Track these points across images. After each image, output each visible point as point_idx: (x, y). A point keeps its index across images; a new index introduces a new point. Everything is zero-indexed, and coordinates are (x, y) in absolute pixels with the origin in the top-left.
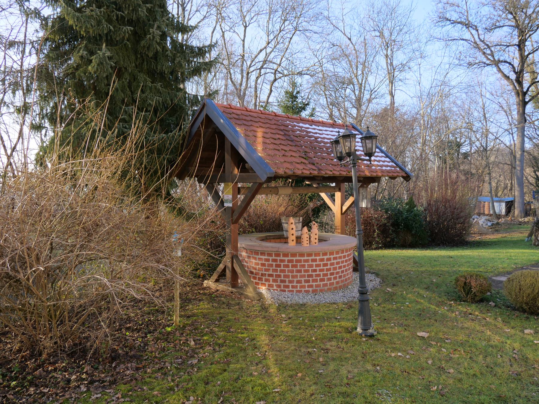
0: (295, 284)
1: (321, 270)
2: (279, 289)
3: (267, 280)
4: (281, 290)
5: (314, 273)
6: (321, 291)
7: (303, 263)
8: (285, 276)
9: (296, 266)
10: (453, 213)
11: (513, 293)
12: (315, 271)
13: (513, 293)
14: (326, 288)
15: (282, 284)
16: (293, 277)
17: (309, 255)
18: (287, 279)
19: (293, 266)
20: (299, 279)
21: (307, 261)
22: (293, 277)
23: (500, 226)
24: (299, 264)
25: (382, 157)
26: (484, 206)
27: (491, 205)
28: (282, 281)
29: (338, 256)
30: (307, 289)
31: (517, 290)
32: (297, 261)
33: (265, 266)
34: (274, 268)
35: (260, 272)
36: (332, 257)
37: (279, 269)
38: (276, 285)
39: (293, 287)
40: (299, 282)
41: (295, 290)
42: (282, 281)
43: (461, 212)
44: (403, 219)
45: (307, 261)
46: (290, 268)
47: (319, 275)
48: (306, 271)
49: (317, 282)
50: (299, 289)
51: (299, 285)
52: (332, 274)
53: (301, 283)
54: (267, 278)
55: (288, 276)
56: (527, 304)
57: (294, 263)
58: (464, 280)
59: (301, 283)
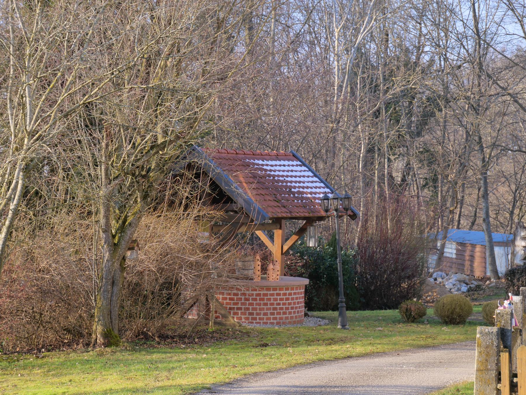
0: (262, 316)
1: (284, 304)
2: (247, 321)
3: (235, 314)
4: (249, 322)
5: (278, 307)
6: (284, 323)
7: (269, 297)
8: (253, 309)
9: (262, 299)
10: (396, 261)
11: (439, 310)
12: (279, 304)
13: (439, 310)
14: (287, 321)
15: (250, 317)
16: (260, 309)
17: (275, 289)
18: (255, 312)
19: (260, 300)
20: (265, 311)
21: (272, 295)
22: (260, 309)
23: (481, 292)
24: (265, 297)
25: (305, 171)
26: (472, 257)
27: (488, 254)
28: (250, 314)
29: (297, 291)
30: (272, 321)
31: (442, 308)
32: (265, 295)
33: (234, 300)
34: (243, 301)
35: (228, 306)
36: (292, 292)
37: (247, 302)
38: (245, 318)
39: (260, 319)
40: (265, 314)
41: (262, 321)
42: (250, 314)
43: (408, 259)
44: (326, 268)
45: (272, 295)
46: (258, 302)
47: (281, 309)
48: (272, 304)
49: (280, 315)
50: (265, 321)
51: (265, 317)
52: (292, 308)
53: (267, 315)
54: (236, 311)
55: (255, 309)
56: (448, 317)
57: (262, 297)
58: (406, 306)
59: (267, 315)
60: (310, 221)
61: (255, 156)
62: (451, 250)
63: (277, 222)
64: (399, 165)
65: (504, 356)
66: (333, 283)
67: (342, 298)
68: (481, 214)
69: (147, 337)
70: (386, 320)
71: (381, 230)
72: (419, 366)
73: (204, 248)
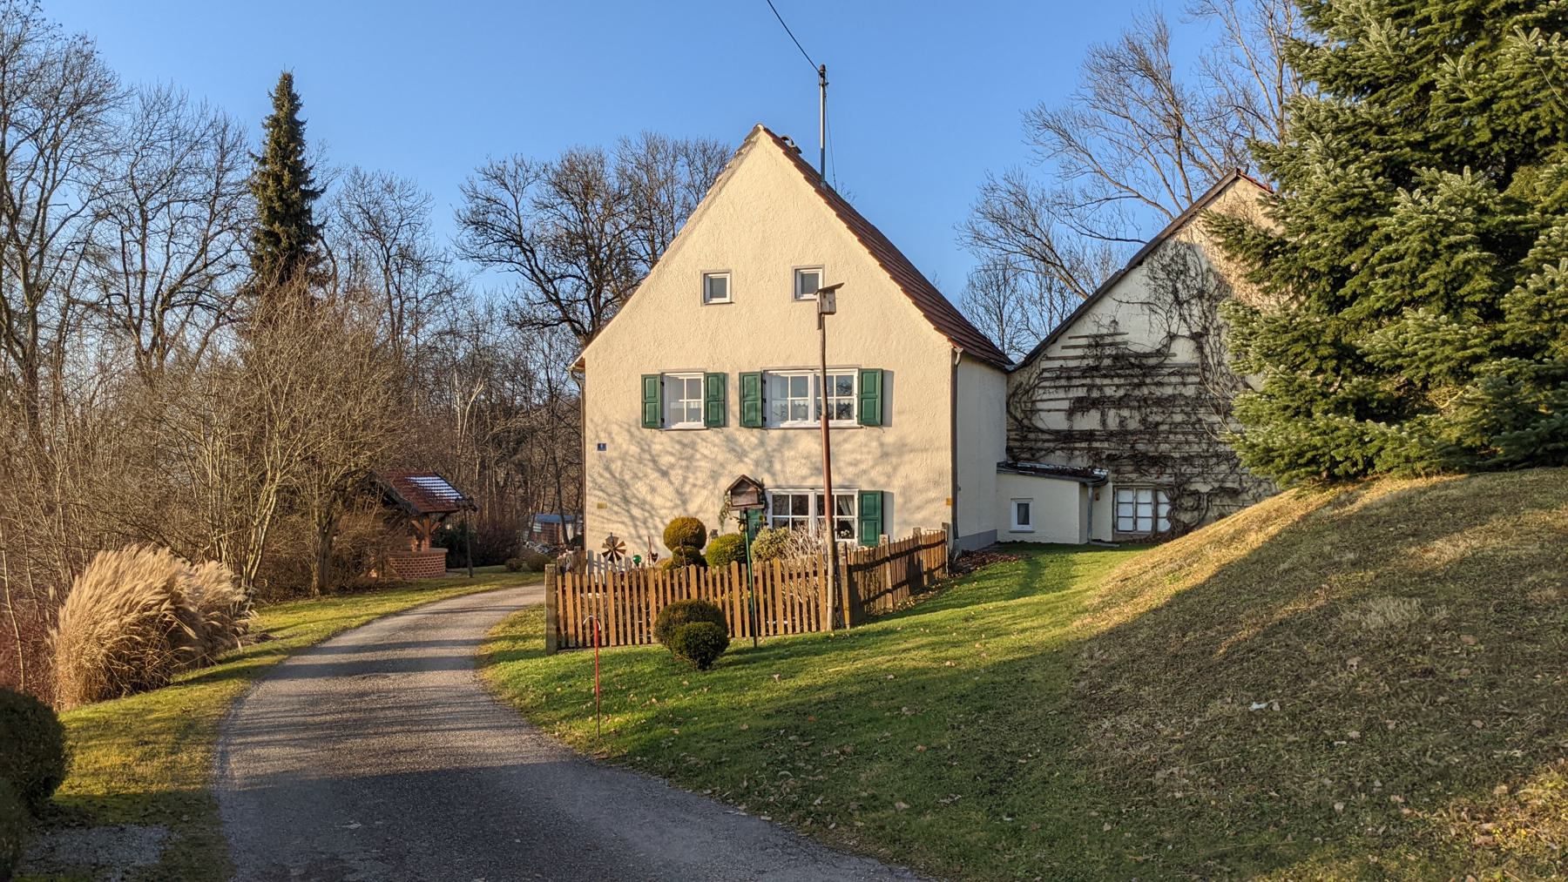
60: (447, 514)
61: (410, 475)
62: (537, 528)
63: (426, 514)
64: (502, 475)
65: (559, 578)
66: (463, 551)
67: (469, 559)
68: (557, 502)
69: (345, 589)
70: (496, 572)
71: (492, 518)
72: (518, 595)
73: (381, 533)
